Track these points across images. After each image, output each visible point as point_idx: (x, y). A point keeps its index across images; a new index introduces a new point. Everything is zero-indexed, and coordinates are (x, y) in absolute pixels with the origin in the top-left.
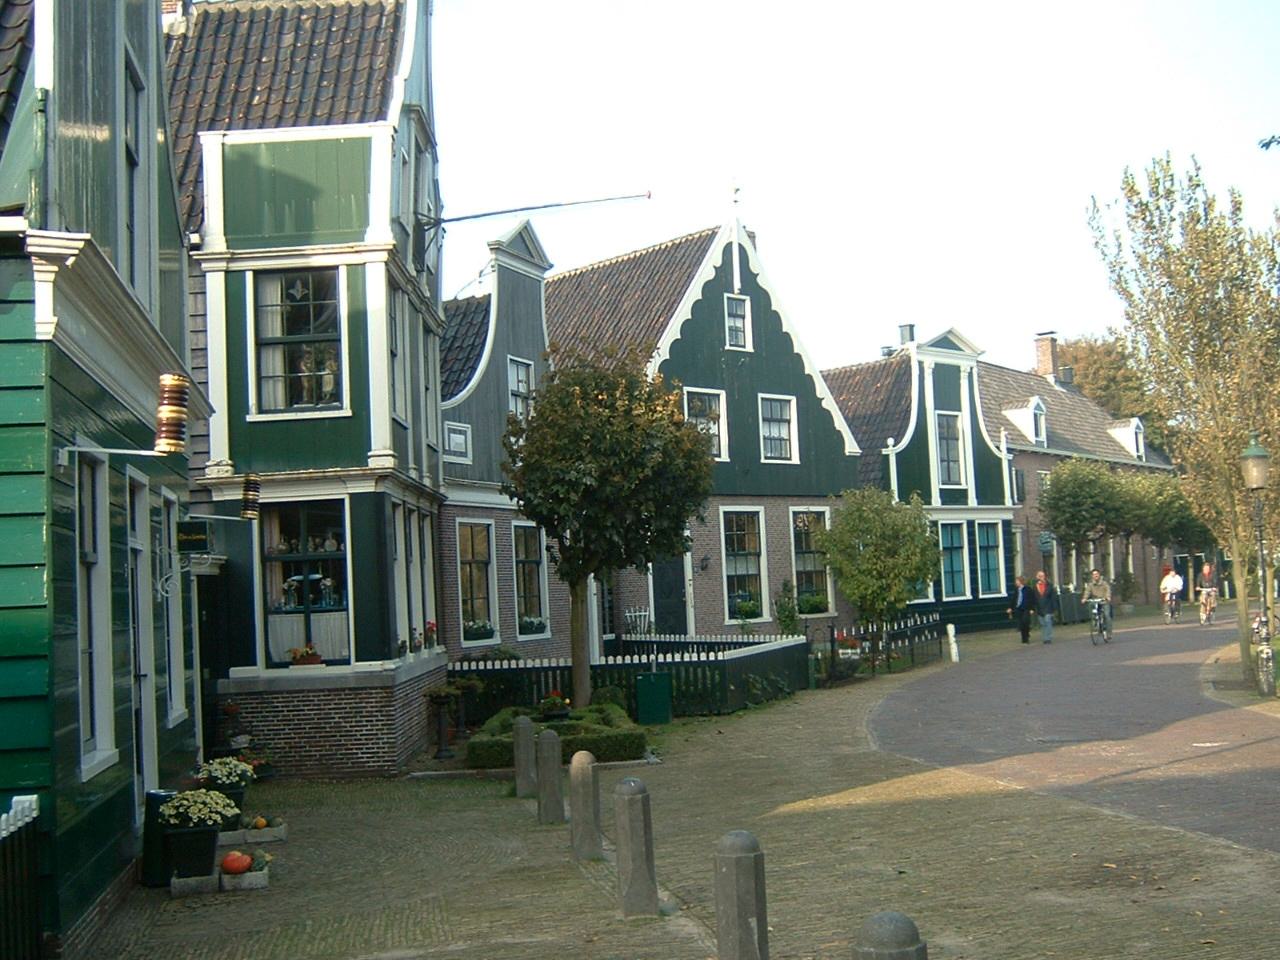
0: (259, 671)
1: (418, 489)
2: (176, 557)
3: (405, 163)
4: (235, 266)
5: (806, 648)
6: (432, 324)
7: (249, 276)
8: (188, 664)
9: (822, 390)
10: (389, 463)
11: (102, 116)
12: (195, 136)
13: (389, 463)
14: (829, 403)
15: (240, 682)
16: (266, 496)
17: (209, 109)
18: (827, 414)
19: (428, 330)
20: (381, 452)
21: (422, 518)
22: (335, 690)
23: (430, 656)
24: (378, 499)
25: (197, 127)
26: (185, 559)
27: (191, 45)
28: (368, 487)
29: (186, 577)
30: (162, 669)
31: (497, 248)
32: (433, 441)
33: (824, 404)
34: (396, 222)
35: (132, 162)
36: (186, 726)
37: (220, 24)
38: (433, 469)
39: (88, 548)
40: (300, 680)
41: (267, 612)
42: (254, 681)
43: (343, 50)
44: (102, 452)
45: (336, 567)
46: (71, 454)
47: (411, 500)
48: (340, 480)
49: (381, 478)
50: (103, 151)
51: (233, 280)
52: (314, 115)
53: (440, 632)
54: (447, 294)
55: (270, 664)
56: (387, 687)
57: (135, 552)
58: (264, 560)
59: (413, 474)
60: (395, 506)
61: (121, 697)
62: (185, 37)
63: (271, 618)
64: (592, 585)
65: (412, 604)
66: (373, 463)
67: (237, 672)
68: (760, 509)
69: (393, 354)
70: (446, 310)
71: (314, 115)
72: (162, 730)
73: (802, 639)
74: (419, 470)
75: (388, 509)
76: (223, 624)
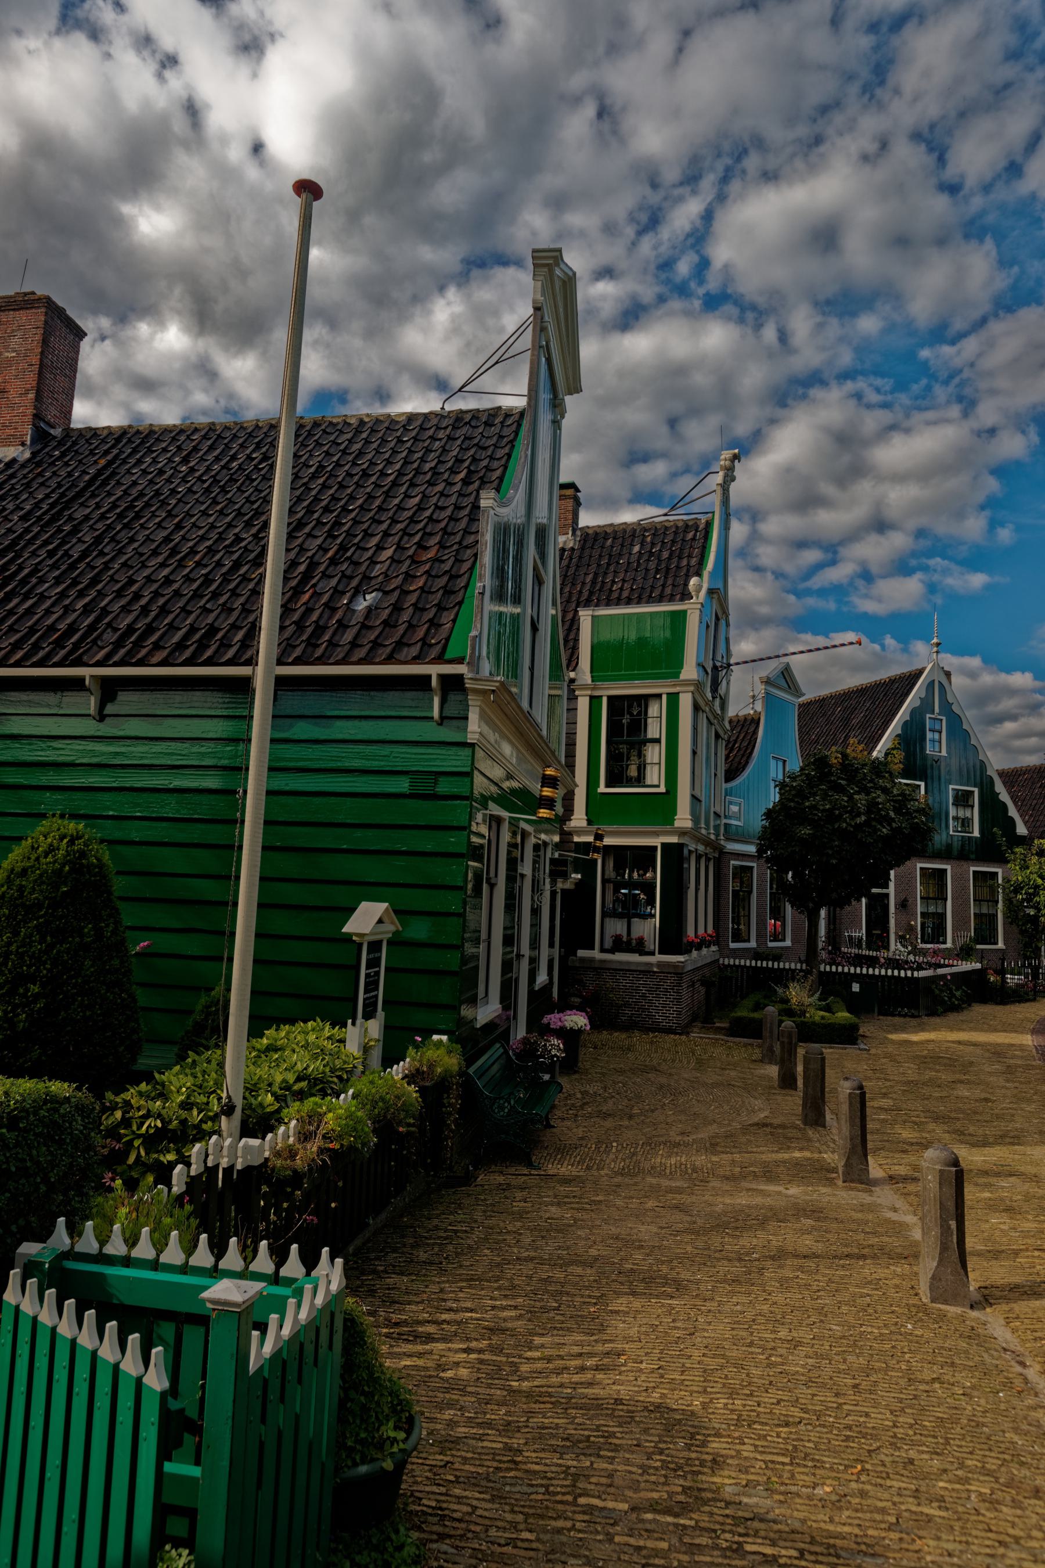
0: (596, 954)
1: (707, 843)
2: (548, 880)
3: (708, 626)
4: (597, 693)
5: (981, 973)
6: (721, 733)
7: (605, 700)
8: (551, 945)
9: (999, 787)
10: (689, 824)
11: (517, 600)
12: (576, 612)
13: (689, 824)
14: (1004, 797)
15: (583, 960)
16: (608, 841)
17: (585, 594)
18: (1012, 820)
19: (717, 736)
20: (683, 819)
21: (708, 860)
22: (646, 972)
23: (708, 953)
24: (680, 846)
25: (578, 606)
26: (553, 882)
27: (576, 554)
28: (674, 840)
29: (553, 894)
30: (535, 944)
31: (768, 682)
32: (718, 809)
33: (1001, 797)
34: (701, 665)
35: (535, 628)
36: (547, 988)
37: (595, 540)
38: (717, 827)
39: (492, 874)
40: (620, 962)
41: (604, 915)
42: (592, 960)
43: (671, 555)
44: (505, 814)
45: (648, 888)
46: (485, 815)
47: (701, 848)
48: (656, 834)
49: (682, 833)
50: (516, 619)
51: (594, 700)
52: (650, 596)
53: (717, 939)
54: (732, 712)
55: (603, 950)
56: (677, 971)
57: (522, 876)
58: (604, 881)
59: (703, 831)
60: (690, 852)
61: (507, 966)
62: (572, 549)
63: (607, 920)
64: (823, 913)
65: (698, 920)
66: (677, 824)
67: (581, 953)
68: (948, 867)
69: (694, 753)
70: (730, 722)
71: (650, 596)
72: (531, 992)
73: (978, 966)
74: (707, 829)
75: (686, 852)
76: (575, 921)
